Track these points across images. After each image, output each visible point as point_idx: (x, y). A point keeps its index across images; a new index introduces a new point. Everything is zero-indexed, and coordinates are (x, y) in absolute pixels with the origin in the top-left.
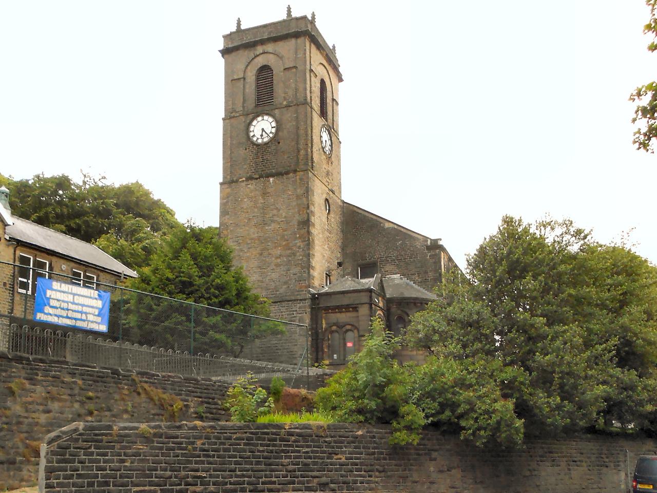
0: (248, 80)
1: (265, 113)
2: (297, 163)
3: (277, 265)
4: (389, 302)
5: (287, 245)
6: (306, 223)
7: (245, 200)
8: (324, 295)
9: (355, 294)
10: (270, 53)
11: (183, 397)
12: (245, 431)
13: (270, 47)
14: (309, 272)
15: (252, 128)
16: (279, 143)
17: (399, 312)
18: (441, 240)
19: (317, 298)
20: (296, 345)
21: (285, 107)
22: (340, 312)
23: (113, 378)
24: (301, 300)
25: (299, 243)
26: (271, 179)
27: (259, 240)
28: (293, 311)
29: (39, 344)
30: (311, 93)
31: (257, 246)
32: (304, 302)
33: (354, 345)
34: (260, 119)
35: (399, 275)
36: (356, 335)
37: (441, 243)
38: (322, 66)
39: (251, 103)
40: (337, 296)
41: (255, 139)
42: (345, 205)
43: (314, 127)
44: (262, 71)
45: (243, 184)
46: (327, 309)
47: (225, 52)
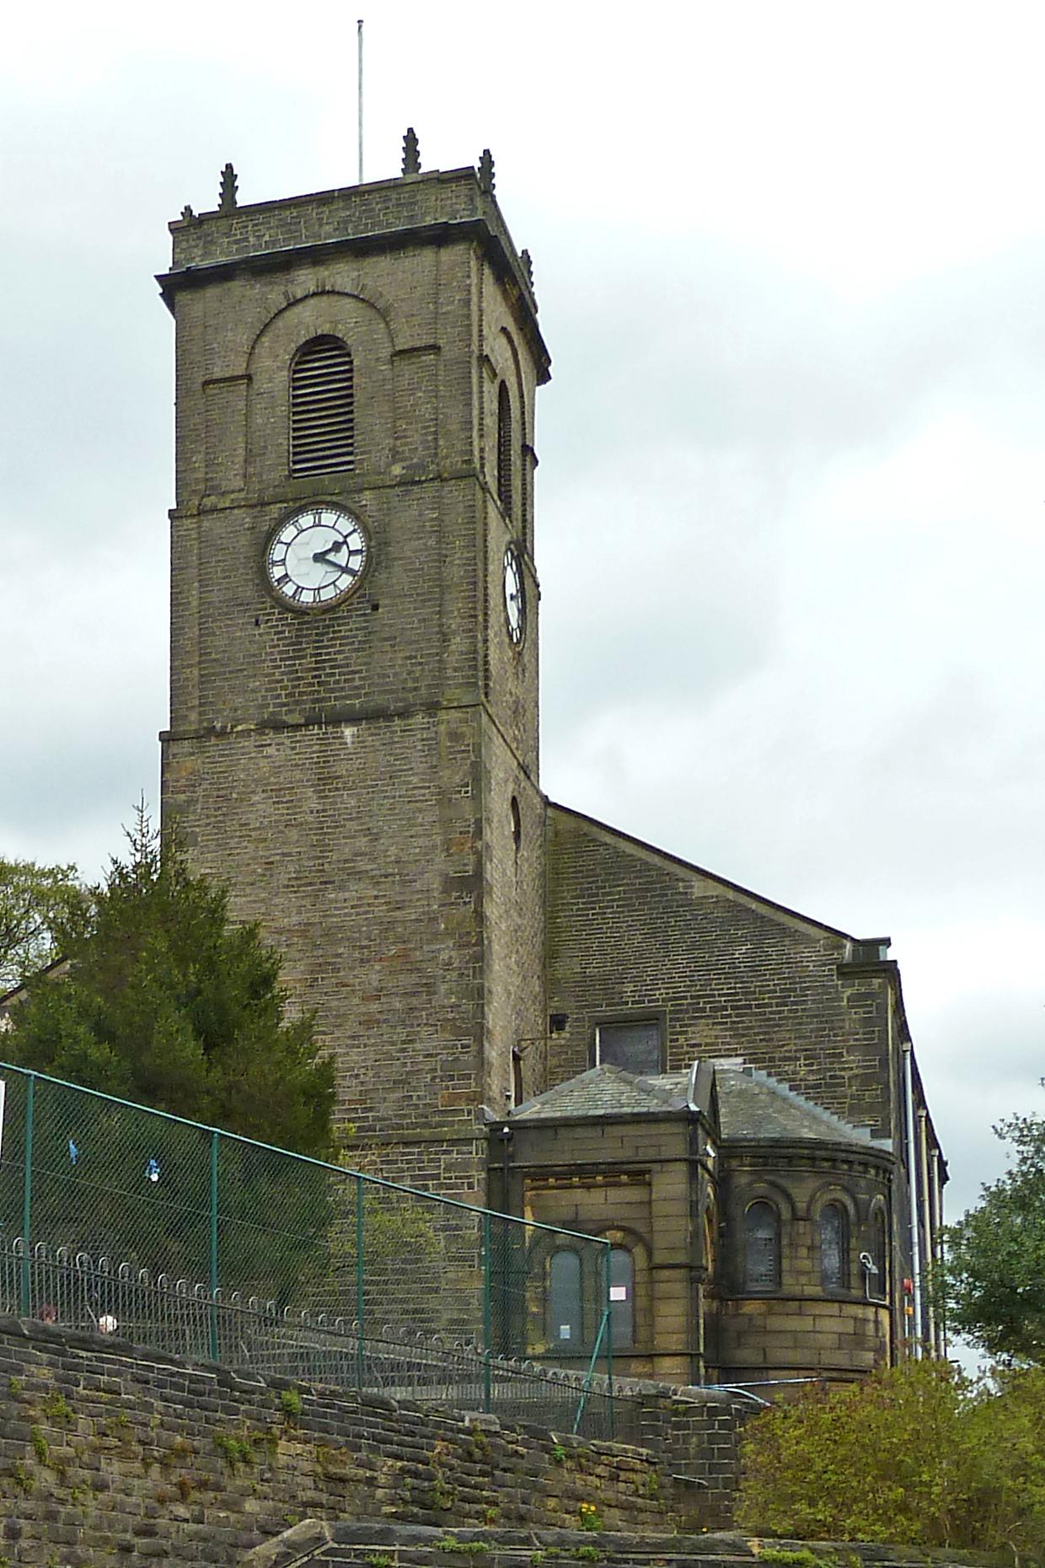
0: (261, 384)
1: (322, 502)
2: (440, 682)
3: (369, 1023)
4: (729, 1150)
5: (404, 956)
6: (472, 884)
7: (256, 798)
8: (535, 1128)
9: (643, 1129)
10: (346, 294)
11: (363, 1455)
12: (667, 1557)
13: (342, 274)
14: (481, 1051)
15: (278, 552)
16: (375, 608)
17: (761, 1187)
18: (887, 942)
19: (510, 1137)
20: (437, 1291)
21: (399, 484)
22: (588, 1187)
23: (222, 1396)
24: (454, 1142)
25: (447, 952)
26: (348, 732)
27: (303, 934)
28: (425, 1177)
29: (41, 1298)
30: (481, 436)
31: (298, 956)
32: (465, 1149)
33: (632, 1294)
34: (306, 520)
35: (740, 1060)
36: (642, 1263)
37: (891, 954)
38: (504, 341)
39: (274, 468)
40: (580, 1132)
41: (289, 589)
42: (550, 812)
43: (491, 554)
44: (305, 354)
45: (248, 743)
46: (541, 1174)
47: (174, 287)
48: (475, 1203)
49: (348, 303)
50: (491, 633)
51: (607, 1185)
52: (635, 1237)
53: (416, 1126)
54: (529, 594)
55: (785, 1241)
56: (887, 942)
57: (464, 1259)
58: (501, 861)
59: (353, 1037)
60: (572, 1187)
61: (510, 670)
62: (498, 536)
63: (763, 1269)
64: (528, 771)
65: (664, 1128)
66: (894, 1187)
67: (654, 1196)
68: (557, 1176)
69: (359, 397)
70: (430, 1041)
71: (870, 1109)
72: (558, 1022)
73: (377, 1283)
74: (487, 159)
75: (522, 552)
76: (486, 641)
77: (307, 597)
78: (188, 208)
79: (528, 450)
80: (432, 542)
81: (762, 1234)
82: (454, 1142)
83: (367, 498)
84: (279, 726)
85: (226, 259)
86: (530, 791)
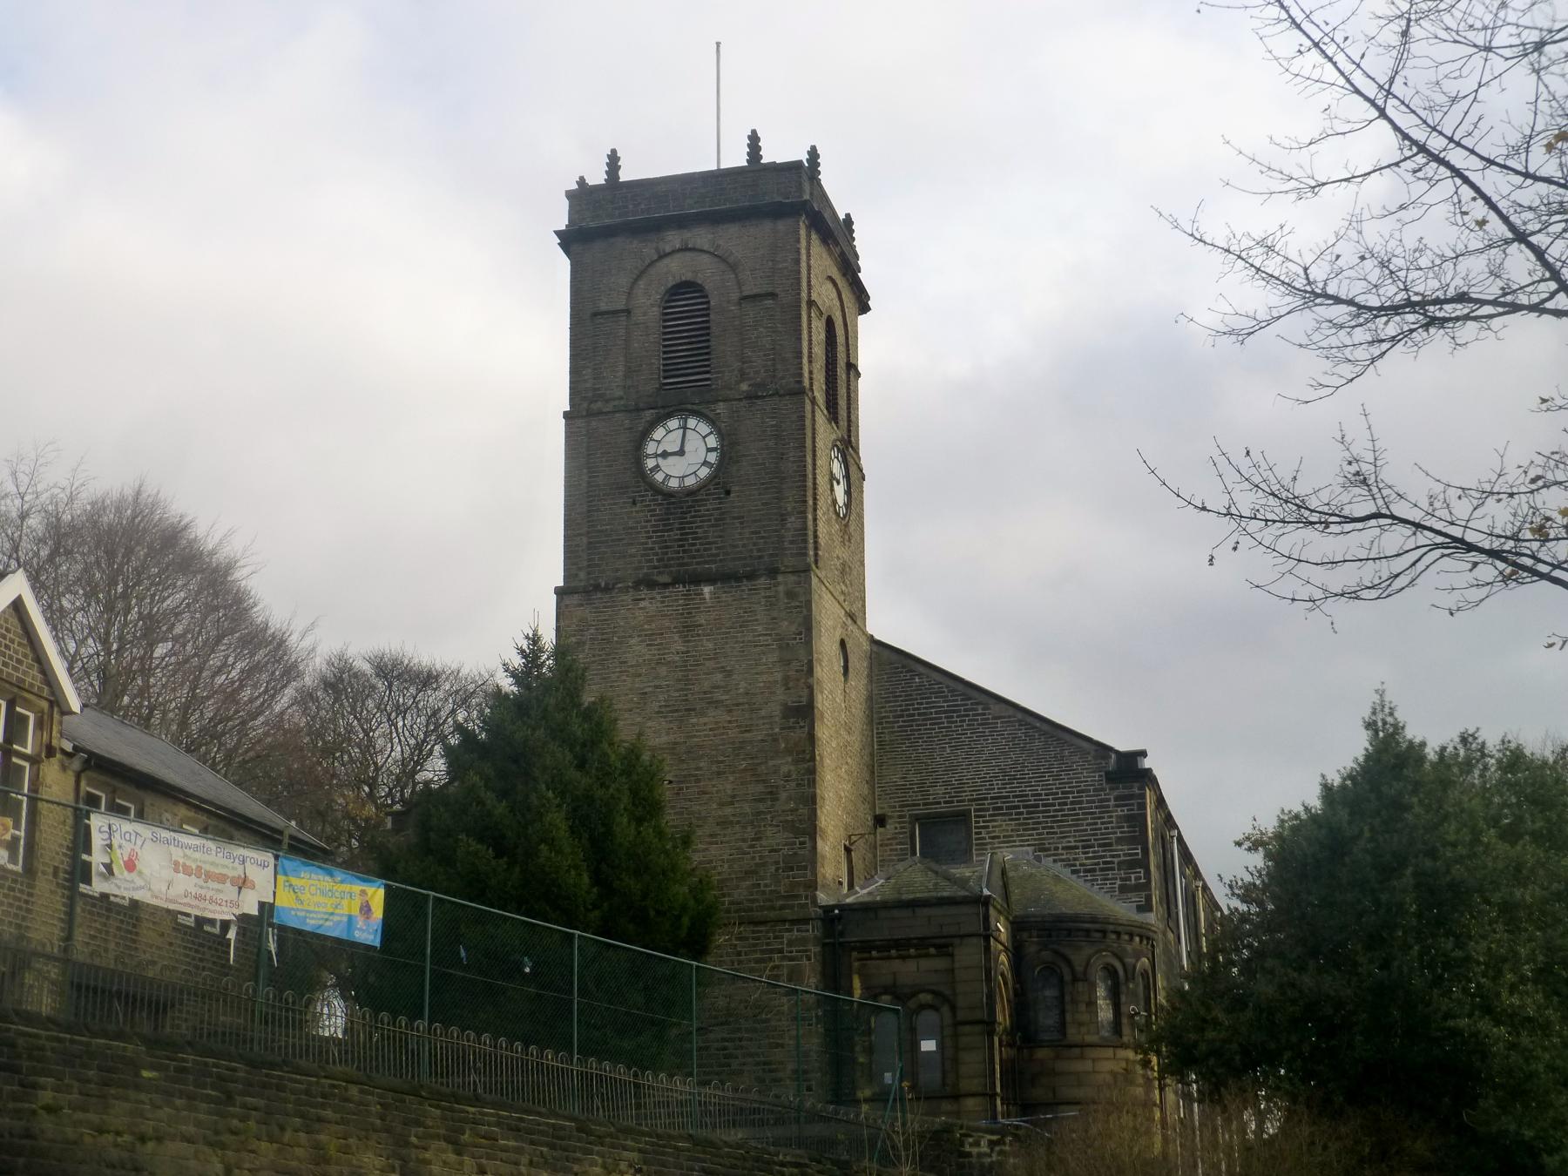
3: (724, 823)
6: (804, 712)
7: (633, 641)
13: (701, 237)
16: (728, 493)
18: (1143, 754)
19: (839, 917)
22: (903, 958)
23: (579, 1140)
24: (794, 922)
25: (786, 765)
28: (772, 951)
30: (810, 362)
33: (941, 1046)
36: (948, 1019)
37: (1147, 763)
38: (830, 286)
43: (819, 453)
45: (628, 598)
48: (811, 983)
49: (705, 258)
50: (820, 513)
51: (918, 956)
52: (944, 999)
53: (762, 908)
54: (854, 477)
55: (1067, 998)
56: (1143, 754)
57: (804, 1019)
58: (831, 692)
59: (711, 836)
60: (889, 958)
61: (837, 539)
62: (825, 434)
63: (1050, 1022)
64: (856, 616)
65: (965, 909)
66: (1157, 951)
67: (957, 965)
68: (879, 949)
69: (714, 329)
70: (775, 837)
71: (1138, 888)
72: (880, 821)
73: (732, 1040)
74: (813, 154)
75: (848, 447)
76: (815, 520)
77: (674, 483)
78: (582, 178)
79: (852, 368)
80: (771, 444)
81: (1050, 993)
82: (794, 922)
83: (721, 408)
84: (651, 585)
85: (613, 226)
86: (857, 632)
